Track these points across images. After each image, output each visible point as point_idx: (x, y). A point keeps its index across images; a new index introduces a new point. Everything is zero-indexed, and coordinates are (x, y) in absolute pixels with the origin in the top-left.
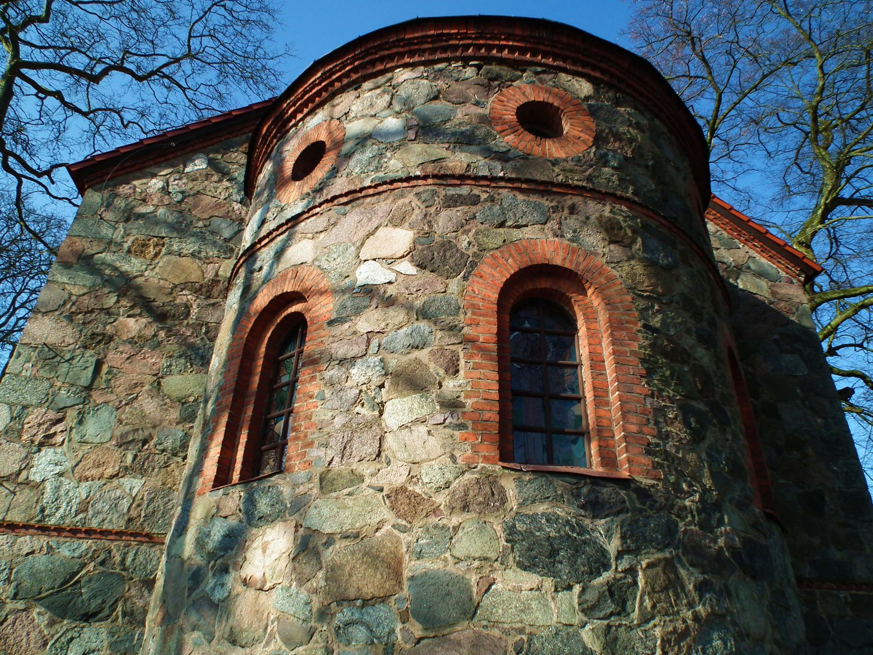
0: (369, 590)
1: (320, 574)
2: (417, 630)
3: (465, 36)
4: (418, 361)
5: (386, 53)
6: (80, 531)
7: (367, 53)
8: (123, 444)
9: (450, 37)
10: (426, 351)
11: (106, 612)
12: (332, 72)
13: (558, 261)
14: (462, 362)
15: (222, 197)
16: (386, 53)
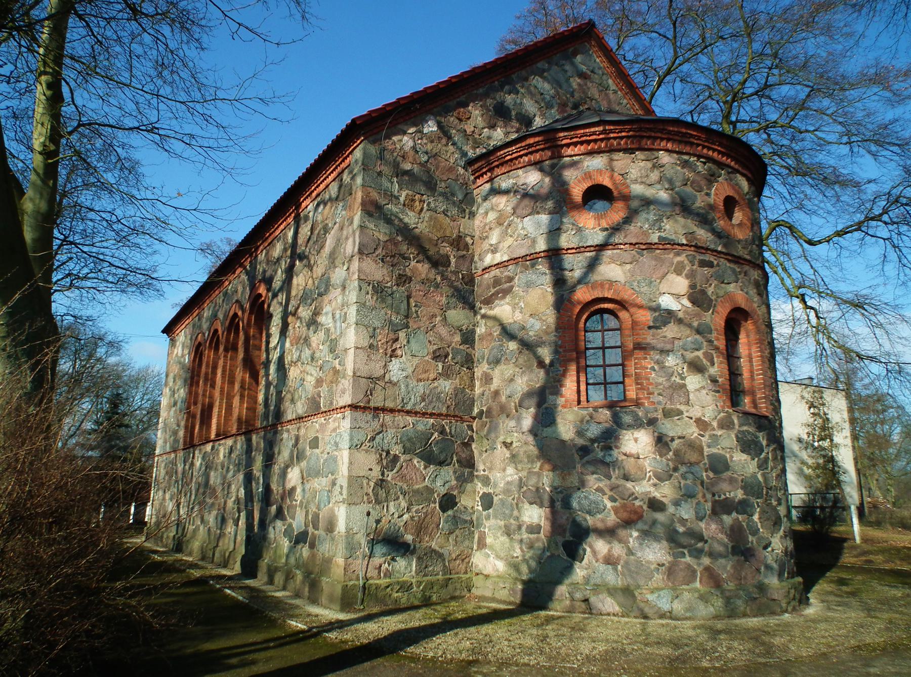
0: (693, 460)
1: (671, 453)
2: (711, 475)
3: (699, 138)
4: (698, 357)
5: (653, 134)
6: (427, 414)
7: (640, 130)
8: (436, 357)
9: (692, 136)
10: (702, 351)
11: (449, 460)
12: (611, 131)
13: (743, 306)
14: (715, 359)
15: (452, 161)
16: (653, 134)
